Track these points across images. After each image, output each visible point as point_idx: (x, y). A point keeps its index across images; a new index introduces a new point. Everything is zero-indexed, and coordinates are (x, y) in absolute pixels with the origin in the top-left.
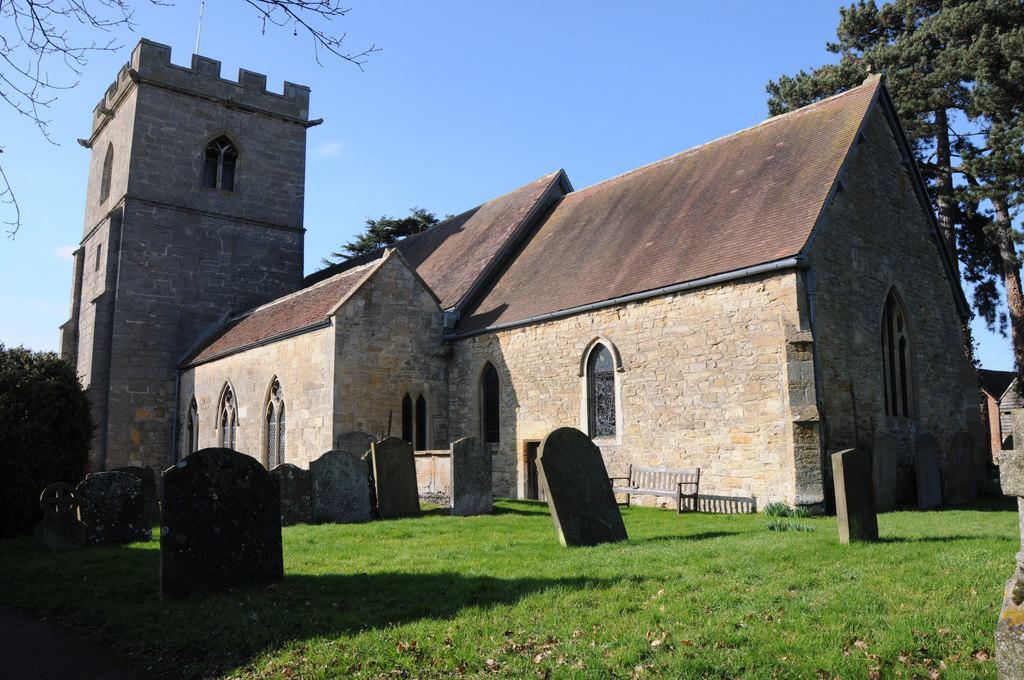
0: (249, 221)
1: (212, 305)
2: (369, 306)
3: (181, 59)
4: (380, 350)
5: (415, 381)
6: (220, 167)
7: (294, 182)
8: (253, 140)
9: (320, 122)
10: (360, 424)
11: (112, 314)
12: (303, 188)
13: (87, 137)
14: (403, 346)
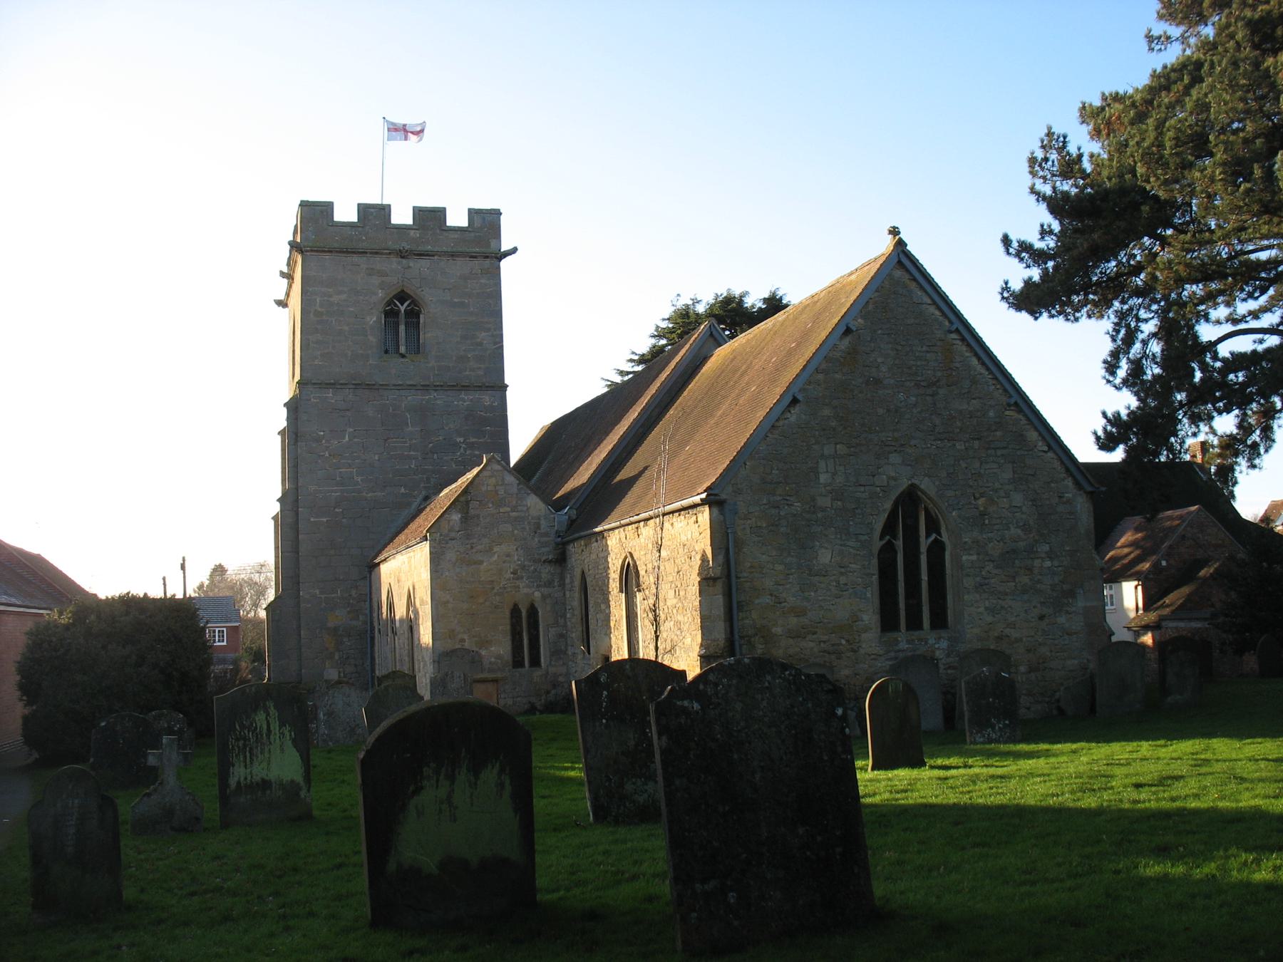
0: (437, 388)
1: (403, 490)
2: (466, 519)
3: (346, 213)
4: (481, 562)
5: (526, 590)
6: (402, 328)
7: (489, 330)
8: (436, 288)
9: (514, 250)
10: (463, 640)
11: (297, 514)
12: (501, 336)
13: (282, 297)
14: (508, 555)
